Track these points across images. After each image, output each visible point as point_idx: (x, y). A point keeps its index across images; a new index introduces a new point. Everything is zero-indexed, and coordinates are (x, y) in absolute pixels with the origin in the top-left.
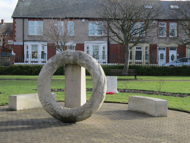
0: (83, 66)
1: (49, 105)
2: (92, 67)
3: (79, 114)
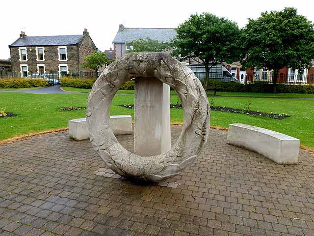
0: (166, 82)
1: (105, 151)
2: (183, 84)
3: (156, 171)
